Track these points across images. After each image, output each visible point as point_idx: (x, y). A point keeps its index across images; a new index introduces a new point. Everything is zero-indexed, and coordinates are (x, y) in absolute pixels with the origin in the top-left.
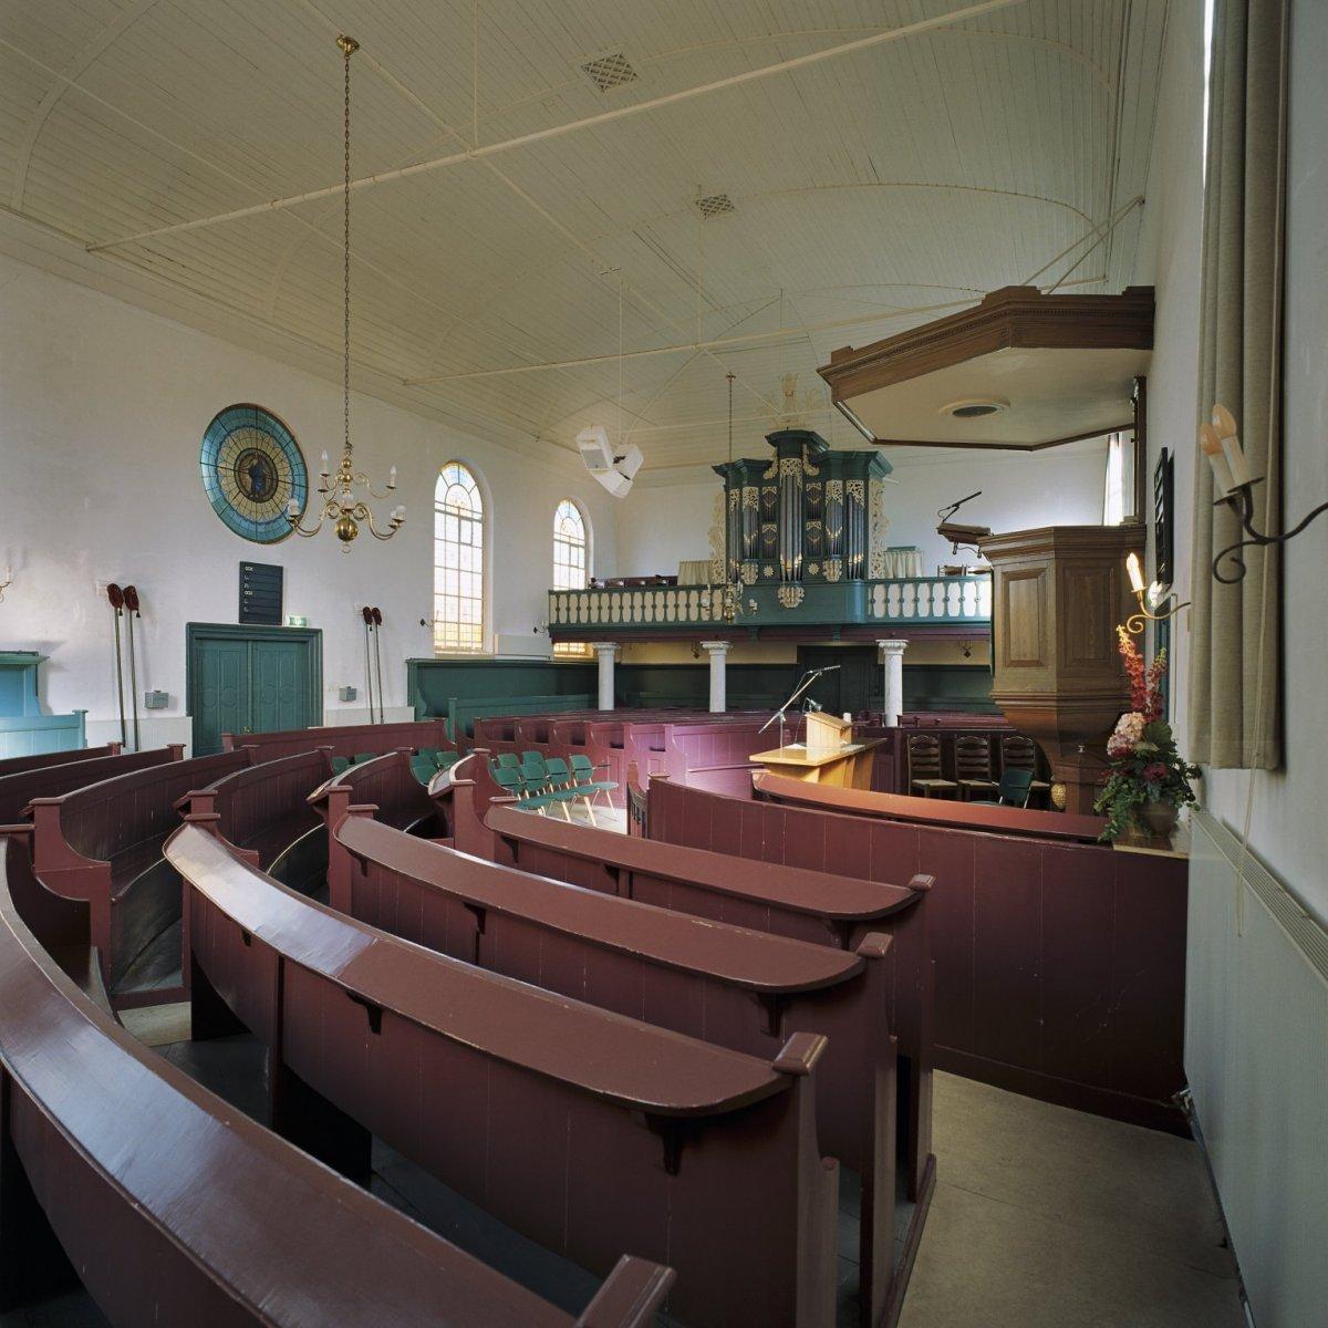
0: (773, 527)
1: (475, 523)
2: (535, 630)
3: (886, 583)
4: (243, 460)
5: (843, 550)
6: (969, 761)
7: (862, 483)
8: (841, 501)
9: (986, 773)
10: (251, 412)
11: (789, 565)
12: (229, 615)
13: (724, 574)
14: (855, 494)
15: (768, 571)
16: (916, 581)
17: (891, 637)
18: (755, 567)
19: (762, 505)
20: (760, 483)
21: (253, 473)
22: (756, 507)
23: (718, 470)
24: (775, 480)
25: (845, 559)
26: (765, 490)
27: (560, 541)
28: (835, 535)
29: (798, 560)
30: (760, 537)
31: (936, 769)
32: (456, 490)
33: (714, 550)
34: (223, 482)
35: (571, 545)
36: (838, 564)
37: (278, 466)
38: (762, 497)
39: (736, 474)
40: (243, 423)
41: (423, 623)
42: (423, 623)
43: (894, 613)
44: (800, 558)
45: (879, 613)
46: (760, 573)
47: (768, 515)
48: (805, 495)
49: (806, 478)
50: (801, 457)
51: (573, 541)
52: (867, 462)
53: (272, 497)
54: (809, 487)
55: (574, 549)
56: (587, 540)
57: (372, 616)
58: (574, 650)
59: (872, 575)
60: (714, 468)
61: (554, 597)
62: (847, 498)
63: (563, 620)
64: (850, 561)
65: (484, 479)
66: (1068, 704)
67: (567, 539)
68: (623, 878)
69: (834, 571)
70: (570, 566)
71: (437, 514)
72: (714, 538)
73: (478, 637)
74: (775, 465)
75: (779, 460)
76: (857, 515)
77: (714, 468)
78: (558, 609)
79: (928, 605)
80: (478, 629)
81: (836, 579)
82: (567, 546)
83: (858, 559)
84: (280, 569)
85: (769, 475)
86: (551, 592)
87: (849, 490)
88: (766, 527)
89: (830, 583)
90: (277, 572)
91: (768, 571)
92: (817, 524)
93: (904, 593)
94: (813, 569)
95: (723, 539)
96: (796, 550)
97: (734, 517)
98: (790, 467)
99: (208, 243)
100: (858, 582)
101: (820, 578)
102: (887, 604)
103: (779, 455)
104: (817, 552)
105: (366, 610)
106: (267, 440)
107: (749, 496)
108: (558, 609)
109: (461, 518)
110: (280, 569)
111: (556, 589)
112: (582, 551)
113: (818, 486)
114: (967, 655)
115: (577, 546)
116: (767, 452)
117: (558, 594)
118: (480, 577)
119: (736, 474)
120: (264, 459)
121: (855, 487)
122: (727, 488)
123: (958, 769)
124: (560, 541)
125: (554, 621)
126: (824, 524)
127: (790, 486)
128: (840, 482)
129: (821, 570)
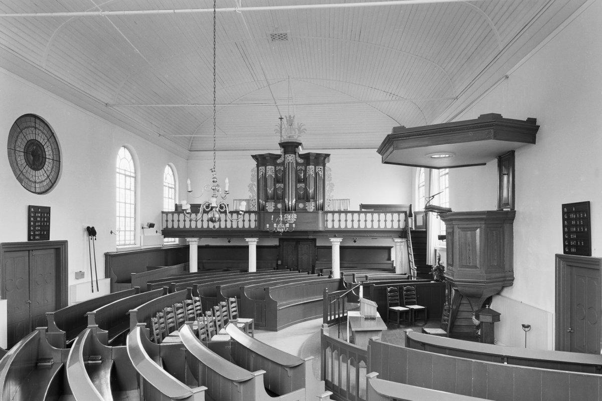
0: (282, 185)
1: (131, 178)
2: (157, 232)
3: (333, 212)
4: (28, 147)
5: (314, 198)
6: (410, 297)
7: (322, 167)
8: (314, 175)
9: (415, 302)
10: (33, 119)
11: (290, 203)
12: (22, 236)
13: (256, 206)
14: (320, 172)
15: (279, 206)
16: (346, 212)
17: (335, 236)
18: (273, 204)
19: (276, 175)
20: (276, 165)
21: (34, 154)
22: (273, 176)
23: (254, 157)
24: (283, 164)
25: (315, 201)
26: (278, 168)
27: (120, 173)
28: (311, 191)
29: (294, 201)
30: (275, 189)
31: (396, 301)
32: (124, 160)
33: (251, 194)
34: (18, 159)
35: (126, 175)
36: (313, 204)
37: (46, 150)
38: (276, 171)
39: (262, 160)
40: (24, 126)
41: (111, 232)
42: (111, 232)
43: (336, 226)
44: (295, 200)
45: (330, 226)
46: (276, 206)
47: (280, 179)
48: (297, 173)
49: (297, 164)
50: (295, 154)
51: (127, 173)
52: (325, 158)
53: (43, 168)
54: (299, 168)
55: (170, 189)
56: (175, 185)
57: (91, 232)
58: (172, 242)
59: (327, 209)
60: (252, 156)
61: (164, 215)
62: (316, 174)
63: (170, 226)
64: (318, 202)
65: (136, 156)
66: (489, 284)
67: (123, 172)
68: (505, 359)
69: (311, 207)
70: (125, 189)
71: (118, 175)
72: (251, 190)
73: (132, 238)
74: (283, 157)
75: (284, 155)
76: (320, 181)
77: (252, 156)
78: (167, 221)
79: (357, 223)
80: (132, 233)
81: (312, 210)
82: (124, 176)
83: (321, 201)
84: (49, 208)
85: (279, 161)
86: (163, 212)
87: (317, 171)
88: (278, 185)
89: (308, 212)
90: (46, 211)
91: (279, 206)
92: (302, 185)
93: (334, 217)
94: (301, 206)
95: (256, 189)
96: (293, 197)
97: (262, 182)
98: (290, 158)
99: (35, 32)
100: (320, 212)
101: (304, 210)
102: (332, 222)
103: (285, 153)
104: (305, 197)
105: (88, 228)
106: (40, 135)
107: (270, 170)
108: (167, 221)
109: (126, 175)
110: (49, 208)
111: (165, 210)
112: (133, 179)
113: (303, 168)
114: (355, 242)
115: (130, 176)
116: (279, 151)
117: (167, 213)
118: (134, 206)
119: (262, 160)
120: (40, 146)
121: (319, 168)
122: (258, 166)
123: (405, 301)
124: (120, 173)
125: (165, 226)
126: (306, 185)
127: (290, 166)
128: (264, 167)
129: (305, 206)
